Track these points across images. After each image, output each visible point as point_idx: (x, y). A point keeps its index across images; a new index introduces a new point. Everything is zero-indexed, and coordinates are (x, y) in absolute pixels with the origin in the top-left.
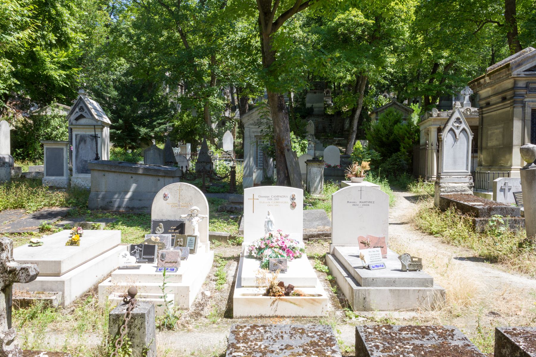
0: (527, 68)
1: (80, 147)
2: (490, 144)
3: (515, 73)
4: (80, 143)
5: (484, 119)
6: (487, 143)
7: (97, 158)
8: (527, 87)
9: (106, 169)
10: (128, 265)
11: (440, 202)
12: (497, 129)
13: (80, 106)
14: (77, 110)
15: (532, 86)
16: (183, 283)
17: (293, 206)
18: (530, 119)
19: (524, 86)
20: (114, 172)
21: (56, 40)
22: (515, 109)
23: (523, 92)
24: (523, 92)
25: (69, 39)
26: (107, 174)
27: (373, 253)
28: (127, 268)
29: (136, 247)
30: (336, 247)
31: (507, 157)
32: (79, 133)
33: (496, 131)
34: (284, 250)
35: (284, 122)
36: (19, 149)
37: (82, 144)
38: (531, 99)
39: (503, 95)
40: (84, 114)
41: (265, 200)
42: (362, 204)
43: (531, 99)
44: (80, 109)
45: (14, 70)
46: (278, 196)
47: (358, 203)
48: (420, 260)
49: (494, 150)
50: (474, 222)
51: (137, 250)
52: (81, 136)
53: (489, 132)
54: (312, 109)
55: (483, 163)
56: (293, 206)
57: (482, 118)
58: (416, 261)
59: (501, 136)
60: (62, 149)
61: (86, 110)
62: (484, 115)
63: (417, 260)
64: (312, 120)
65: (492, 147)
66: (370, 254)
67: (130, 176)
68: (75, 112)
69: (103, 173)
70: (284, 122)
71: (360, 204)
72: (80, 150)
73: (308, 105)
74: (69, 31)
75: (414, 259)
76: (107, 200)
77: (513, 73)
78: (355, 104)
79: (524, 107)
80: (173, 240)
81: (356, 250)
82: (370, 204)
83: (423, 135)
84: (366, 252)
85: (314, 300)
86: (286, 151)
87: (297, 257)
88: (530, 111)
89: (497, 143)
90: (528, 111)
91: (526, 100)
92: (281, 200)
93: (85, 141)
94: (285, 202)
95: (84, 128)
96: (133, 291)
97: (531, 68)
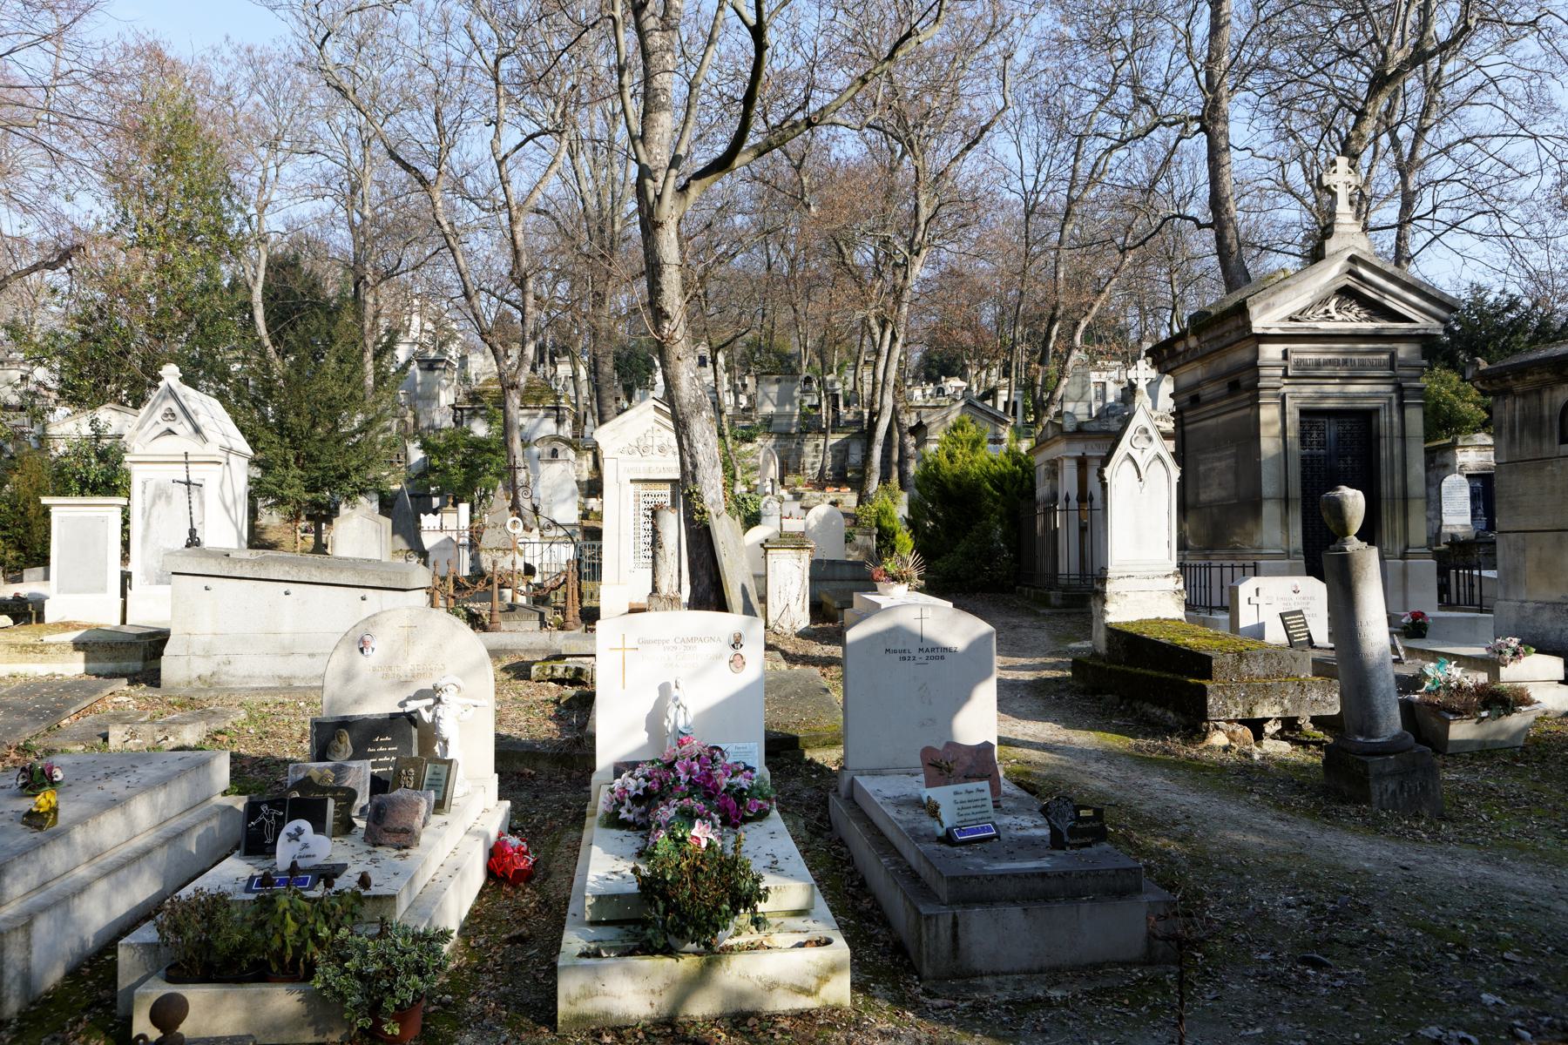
1: (155, 512)
2: (1203, 497)
5: (1188, 437)
6: (1197, 495)
11: (1109, 640)
12: (1220, 459)
27: (965, 797)
29: (264, 808)
30: (857, 778)
31: (1249, 526)
33: (1217, 464)
37: (161, 504)
39: (1233, 378)
42: (924, 655)
47: (915, 652)
49: (1215, 510)
51: (269, 817)
52: (158, 486)
53: (1202, 468)
55: (1190, 543)
57: (1183, 432)
58: (1087, 819)
59: (1230, 477)
62: (1188, 428)
63: (1090, 813)
65: (1210, 504)
66: (959, 798)
71: (918, 655)
72: (153, 521)
75: (1083, 813)
81: (917, 787)
83: (1043, 476)
84: (943, 795)
85: (609, 247)
89: (1223, 494)
90: (1293, 417)
93: (169, 498)
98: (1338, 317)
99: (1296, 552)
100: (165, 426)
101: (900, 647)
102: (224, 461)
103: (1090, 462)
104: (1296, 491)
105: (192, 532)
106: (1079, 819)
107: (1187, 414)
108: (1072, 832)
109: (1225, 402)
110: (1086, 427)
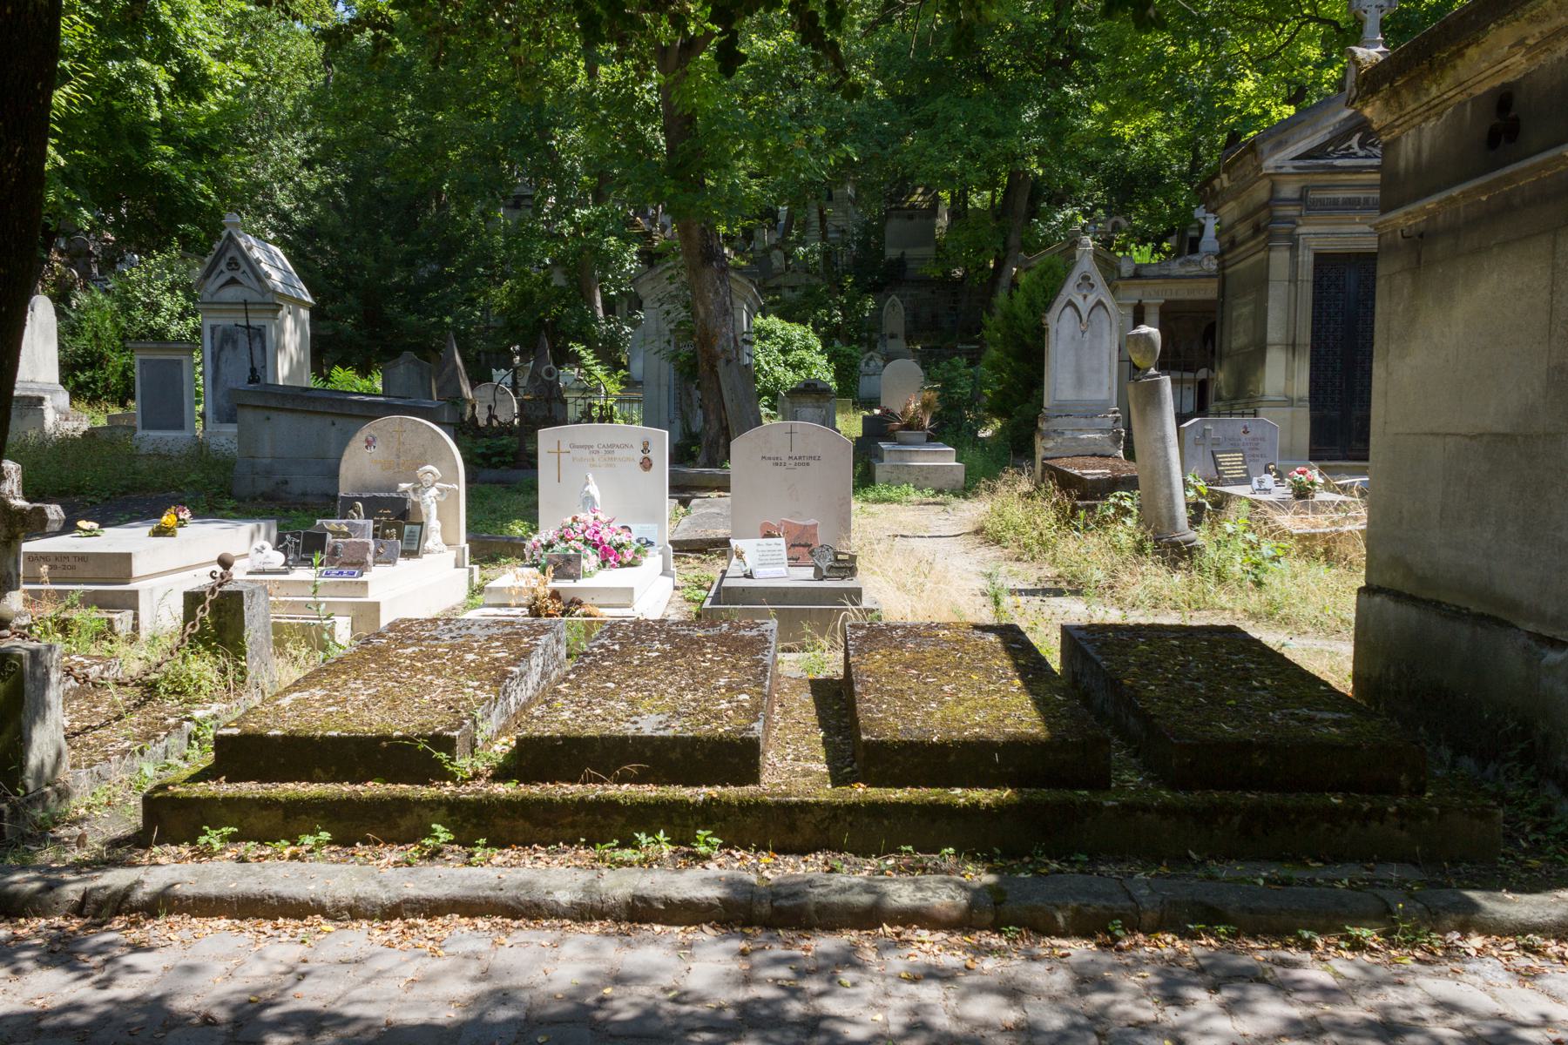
0: (1300, 152)
1: (223, 358)
2: (1234, 345)
3: (1269, 164)
4: (221, 348)
7: (254, 377)
8: (1302, 199)
9: (273, 403)
10: (267, 567)
13: (229, 255)
14: (223, 266)
15: (1313, 195)
16: (371, 597)
17: (646, 464)
18: (1311, 278)
19: (1296, 196)
20: (292, 411)
21: (170, 83)
22: (1272, 254)
23: (1291, 211)
24: (1291, 211)
25: (205, 78)
26: (274, 415)
28: (263, 572)
32: (220, 322)
34: (596, 546)
35: (716, 292)
36: (82, 372)
37: (228, 352)
38: (1312, 229)
40: (238, 275)
41: (586, 453)
43: (1312, 229)
44: (229, 264)
45: (63, 162)
46: (612, 446)
47: (785, 459)
48: (853, 558)
50: (1075, 509)
52: (224, 330)
54: (901, 263)
56: (646, 464)
60: (180, 363)
61: (244, 267)
62: (1228, 271)
64: (901, 297)
67: (329, 420)
68: (217, 271)
69: (267, 413)
70: (716, 292)
72: (222, 366)
73: (892, 253)
74: (205, 58)
76: (279, 477)
77: (1265, 164)
78: (1000, 247)
79: (1294, 249)
80: (376, 529)
82: (811, 462)
86: (721, 364)
87: (630, 565)
88: (1311, 258)
90: (1306, 258)
91: (1300, 230)
92: (618, 453)
93: (235, 343)
94: (628, 459)
95: (221, 310)
96: (228, 559)
97: (1312, 150)
98: (1361, 153)
99: (1300, 400)
100: (227, 276)
101: (773, 455)
102: (1007, 601)
103: (1147, 310)
104: (1305, 336)
105: (253, 370)
106: (837, 560)
107: (1227, 257)
108: (830, 568)
109: (1252, 243)
110: (1144, 272)
